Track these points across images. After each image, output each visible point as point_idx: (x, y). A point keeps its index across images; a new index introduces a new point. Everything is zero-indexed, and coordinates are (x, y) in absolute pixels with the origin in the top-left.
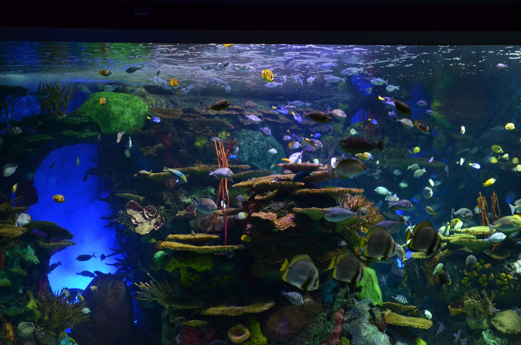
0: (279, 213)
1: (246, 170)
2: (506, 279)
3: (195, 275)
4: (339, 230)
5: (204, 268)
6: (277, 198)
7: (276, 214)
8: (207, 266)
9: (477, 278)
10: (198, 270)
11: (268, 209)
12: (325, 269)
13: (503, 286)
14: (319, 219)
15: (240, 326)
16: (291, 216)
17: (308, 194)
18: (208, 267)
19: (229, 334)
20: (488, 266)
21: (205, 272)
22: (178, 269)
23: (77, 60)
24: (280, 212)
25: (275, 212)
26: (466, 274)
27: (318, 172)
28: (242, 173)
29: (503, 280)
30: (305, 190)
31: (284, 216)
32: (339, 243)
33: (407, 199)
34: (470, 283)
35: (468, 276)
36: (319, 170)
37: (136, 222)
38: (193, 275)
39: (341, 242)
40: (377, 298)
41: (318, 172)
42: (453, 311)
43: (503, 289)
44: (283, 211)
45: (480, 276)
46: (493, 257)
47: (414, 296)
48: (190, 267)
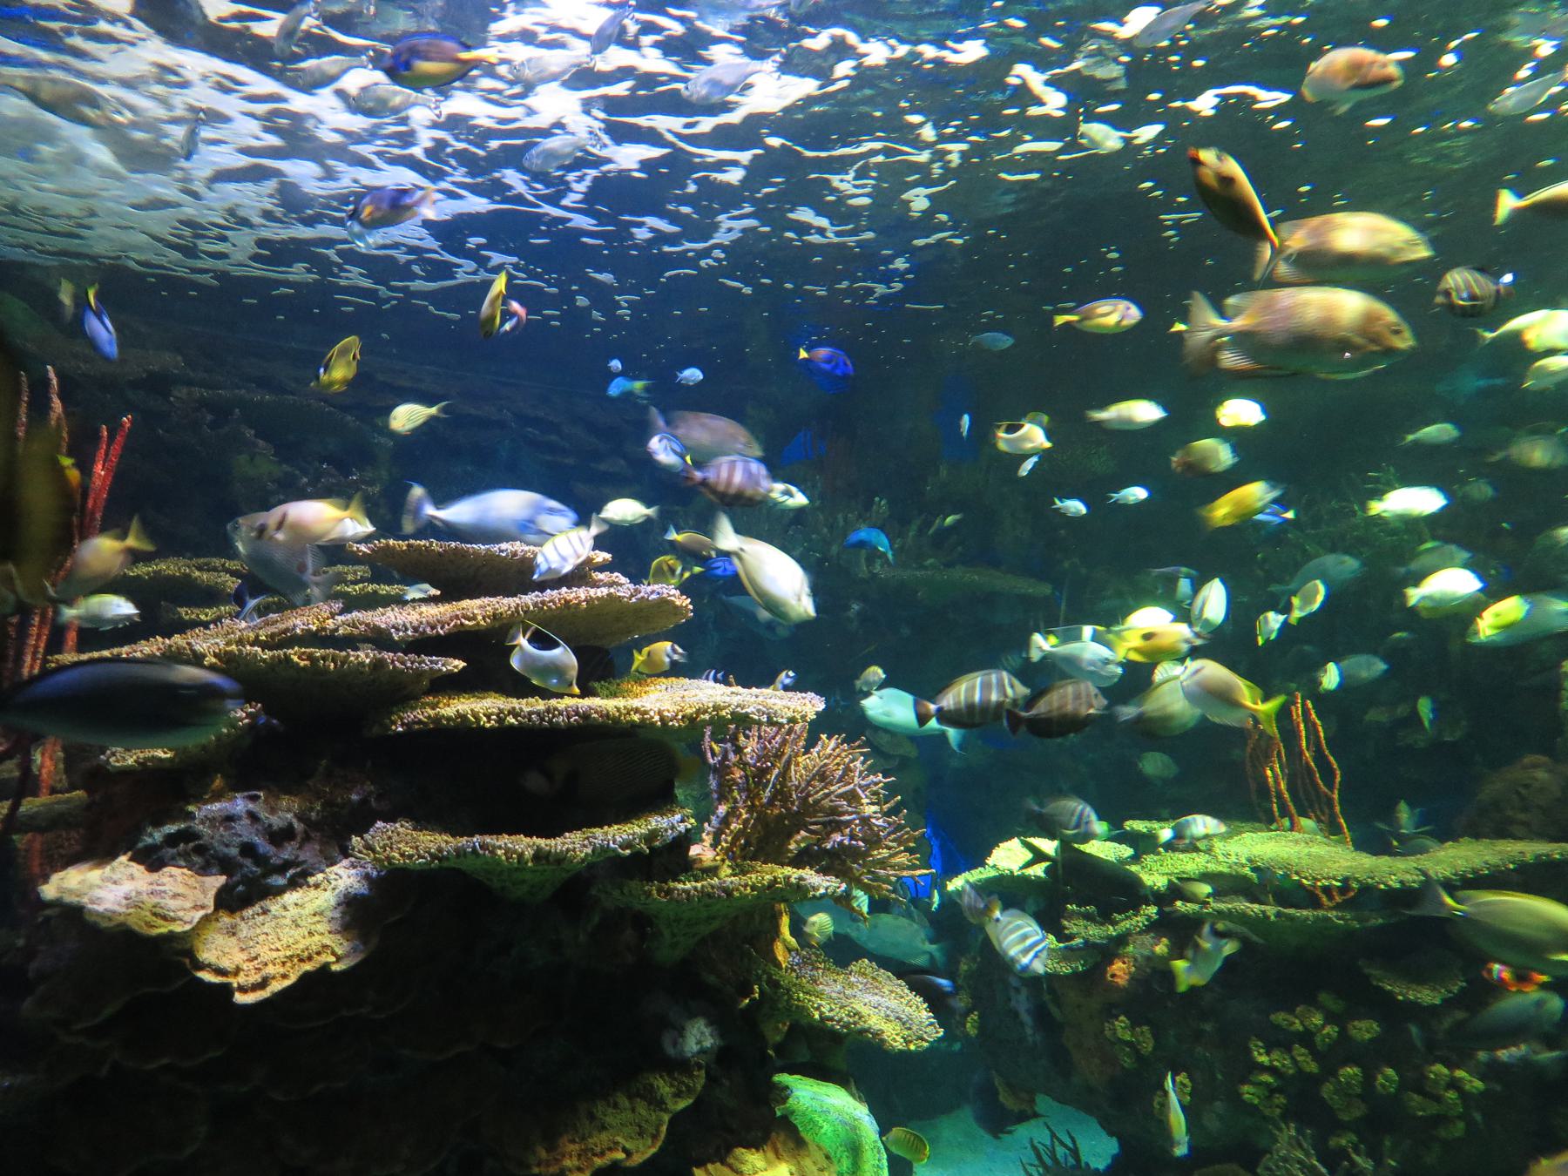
0: (249, 865)
2: (1451, 1095)
6: (251, 764)
9: (1314, 1081)
11: (171, 840)
13: (1440, 1120)
16: (344, 877)
20: (1365, 1030)
24: (260, 860)
25: (203, 858)
26: (1264, 1059)
29: (1438, 1099)
31: (294, 884)
32: (667, 1041)
33: (1397, 309)
34: (1280, 1100)
35: (1272, 1070)
37: (402, 855)
39: (681, 1032)
43: (1442, 1133)
45: (1329, 1072)
46: (1391, 994)
47: (718, 31)
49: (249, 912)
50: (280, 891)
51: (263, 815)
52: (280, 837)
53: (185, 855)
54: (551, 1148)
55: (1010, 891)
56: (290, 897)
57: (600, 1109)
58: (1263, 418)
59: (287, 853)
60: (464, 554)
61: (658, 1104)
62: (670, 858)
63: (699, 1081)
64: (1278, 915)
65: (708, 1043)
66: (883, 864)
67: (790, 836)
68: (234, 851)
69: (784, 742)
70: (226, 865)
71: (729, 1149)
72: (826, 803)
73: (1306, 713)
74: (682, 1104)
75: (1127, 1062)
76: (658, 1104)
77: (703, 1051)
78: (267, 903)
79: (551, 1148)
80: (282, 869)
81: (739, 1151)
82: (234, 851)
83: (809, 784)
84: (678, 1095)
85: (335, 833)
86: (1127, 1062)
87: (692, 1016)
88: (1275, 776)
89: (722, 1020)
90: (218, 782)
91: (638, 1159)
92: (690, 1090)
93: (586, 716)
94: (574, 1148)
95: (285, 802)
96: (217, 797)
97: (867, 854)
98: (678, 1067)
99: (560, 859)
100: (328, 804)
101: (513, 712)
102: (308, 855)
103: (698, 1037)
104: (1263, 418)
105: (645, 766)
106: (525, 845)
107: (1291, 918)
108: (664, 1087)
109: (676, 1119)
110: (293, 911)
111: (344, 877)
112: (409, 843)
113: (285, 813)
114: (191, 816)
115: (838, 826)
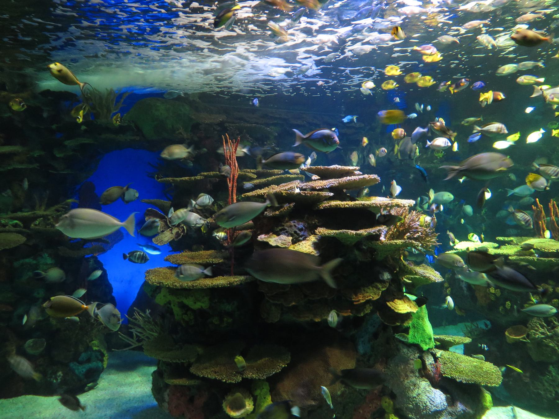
1: (278, 174)
3: (189, 313)
4: (380, 257)
5: (198, 306)
6: (293, 215)
7: (291, 238)
8: (202, 304)
10: (192, 307)
11: (281, 230)
12: (360, 313)
14: (353, 244)
15: (238, 395)
16: (313, 239)
17: (337, 209)
18: (203, 305)
19: (224, 405)
21: (201, 312)
22: (169, 303)
23: (106, 62)
24: (298, 234)
25: (289, 234)
27: (353, 178)
28: (270, 179)
30: (334, 203)
31: (304, 240)
36: (355, 175)
38: (186, 314)
40: (427, 341)
41: (353, 178)
42: (511, 337)
44: (301, 233)
48: (182, 302)
49: (296, 245)
50: (301, 241)
51: (297, 225)
52: (301, 230)
53: (284, 233)
54: (356, 295)
55: (503, 137)
56: (303, 242)
57: (366, 289)
58: (527, 143)
59: (301, 233)
60: (329, 169)
61: (379, 289)
62: (376, 237)
63: (388, 285)
64: (538, 259)
65: (389, 277)
66: (428, 241)
67: (405, 234)
68: (293, 232)
69: (403, 212)
70: (292, 235)
71: (394, 299)
72: (415, 226)
73: (554, 205)
74: (384, 289)
75: (493, 298)
76: (379, 289)
77: (388, 279)
78: (300, 243)
79: (356, 295)
80: (301, 236)
81: (396, 300)
82: (293, 232)
83: (163, 231)
84: (383, 287)
85: (312, 230)
86: (493, 298)
87: (385, 271)
88: (542, 224)
89: (391, 273)
90: (287, 219)
91: (375, 299)
92: (385, 287)
93: (363, 205)
94: (362, 296)
95: (300, 223)
96: (287, 222)
97: (425, 239)
98: (383, 282)
99: (360, 235)
100: (308, 224)
101: (347, 204)
102: (306, 234)
103: (387, 276)
104: (527, 143)
105: (367, 216)
106: (354, 232)
107: (541, 260)
108: (380, 286)
109: (383, 292)
110: (305, 245)
111: (313, 239)
112: (322, 231)
113: (301, 226)
114: (284, 226)
115: (418, 232)
